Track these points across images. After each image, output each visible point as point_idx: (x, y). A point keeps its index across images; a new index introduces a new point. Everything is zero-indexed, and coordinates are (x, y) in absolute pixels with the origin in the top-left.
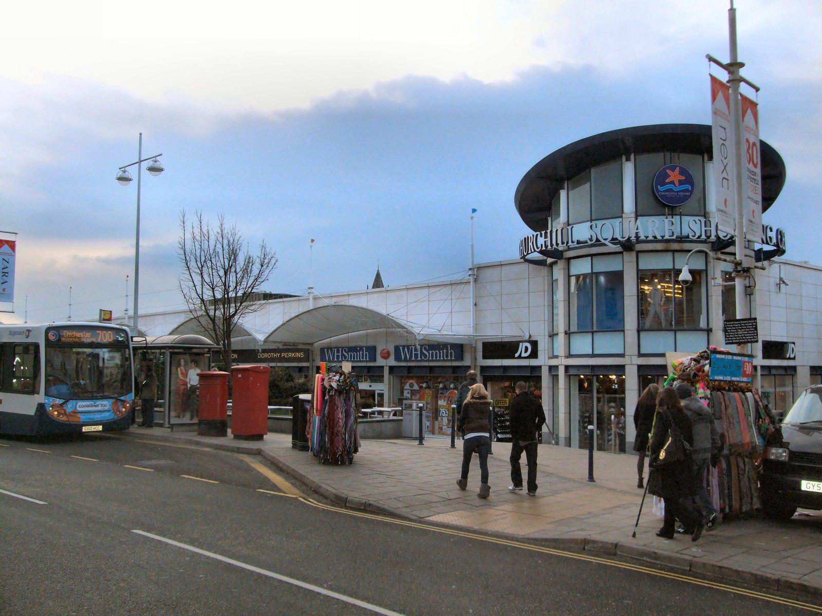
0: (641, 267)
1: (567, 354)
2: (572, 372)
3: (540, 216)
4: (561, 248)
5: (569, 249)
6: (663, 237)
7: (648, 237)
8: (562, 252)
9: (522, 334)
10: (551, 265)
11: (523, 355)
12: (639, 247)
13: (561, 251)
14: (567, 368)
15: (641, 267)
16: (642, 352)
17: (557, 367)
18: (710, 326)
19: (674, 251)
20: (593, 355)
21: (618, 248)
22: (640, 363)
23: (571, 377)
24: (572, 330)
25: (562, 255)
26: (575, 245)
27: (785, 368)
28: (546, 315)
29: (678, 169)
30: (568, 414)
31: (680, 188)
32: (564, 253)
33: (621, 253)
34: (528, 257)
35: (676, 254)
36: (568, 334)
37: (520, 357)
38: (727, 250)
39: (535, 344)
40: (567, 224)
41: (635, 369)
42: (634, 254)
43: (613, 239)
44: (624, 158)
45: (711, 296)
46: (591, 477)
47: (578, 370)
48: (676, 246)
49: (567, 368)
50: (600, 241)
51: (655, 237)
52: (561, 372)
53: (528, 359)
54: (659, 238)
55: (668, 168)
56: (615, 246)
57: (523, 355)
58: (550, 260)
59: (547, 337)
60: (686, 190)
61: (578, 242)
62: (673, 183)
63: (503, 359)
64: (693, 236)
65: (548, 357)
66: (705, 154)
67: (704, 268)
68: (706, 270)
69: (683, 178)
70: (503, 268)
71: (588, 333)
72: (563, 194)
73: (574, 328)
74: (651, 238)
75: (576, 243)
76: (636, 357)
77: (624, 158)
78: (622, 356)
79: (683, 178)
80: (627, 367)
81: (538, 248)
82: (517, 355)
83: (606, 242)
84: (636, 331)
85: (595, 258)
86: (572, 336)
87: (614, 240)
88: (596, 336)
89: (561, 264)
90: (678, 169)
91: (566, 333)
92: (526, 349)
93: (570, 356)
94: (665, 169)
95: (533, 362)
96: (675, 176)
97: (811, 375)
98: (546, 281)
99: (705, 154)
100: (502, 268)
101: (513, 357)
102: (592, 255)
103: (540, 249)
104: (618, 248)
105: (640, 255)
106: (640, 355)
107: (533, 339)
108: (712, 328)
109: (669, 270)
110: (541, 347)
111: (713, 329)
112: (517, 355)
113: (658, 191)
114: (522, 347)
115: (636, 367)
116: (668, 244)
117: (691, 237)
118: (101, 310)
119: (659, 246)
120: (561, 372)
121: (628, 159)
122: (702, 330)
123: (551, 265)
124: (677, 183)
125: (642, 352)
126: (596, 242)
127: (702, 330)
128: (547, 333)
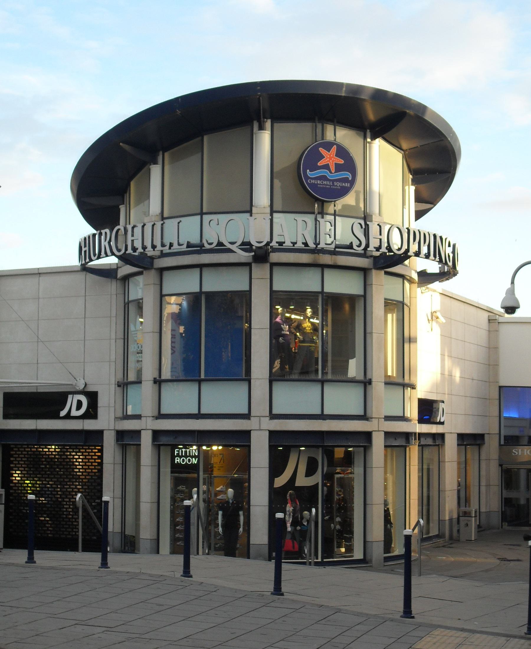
0: (275, 288)
1: (156, 414)
2: (164, 440)
3: (107, 201)
4: (150, 252)
5: (163, 255)
6: (294, 244)
7: (296, 243)
8: (152, 258)
9: (72, 382)
10: (126, 278)
11: (74, 413)
12: (274, 257)
13: (149, 257)
14: (156, 434)
15: (275, 288)
16: (275, 412)
17: (137, 434)
18: (369, 377)
19: (323, 267)
20: (199, 416)
21: (244, 256)
22: (272, 428)
23: (162, 448)
24: (163, 377)
25: (152, 264)
26: (184, 248)
27: (434, 436)
28: (113, 353)
29: (334, 148)
30: (156, 504)
31: (337, 176)
32: (155, 261)
33: (249, 265)
34: (96, 263)
35: (327, 272)
36: (158, 382)
37: (68, 416)
38: (396, 269)
39: (93, 397)
40: (160, 217)
41: (266, 436)
42: (153, 273)
43: (243, 244)
44: (256, 125)
45: (371, 333)
46: (408, 612)
47: (176, 438)
48: (326, 259)
49: (156, 434)
50: (223, 245)
51: (306, 244)
52: (146, 440)
53: (82, 420)
54: (312, 245)
55: (321, 145)
56: (247, 254)
57: (74, 413)
58: (128, 269)
59: (113, 387)
60: (345, 180)
61: (189, 245)
62: (327, 167)
63: (39, 419)
64: (357, 246)
65: (116, 418)
66: (368, 131)
67: (361, 293)
68: (364, 296)
69: (342, 162)
70: (42, 278)
71: (317, 383)
72: (155, 171)
73: (166, 374)
74: (300, 245)
75: (185, 246)
76: (383, 419)
77: (256, 125)
78: (247, 416)
79: (342, 162)
80: (253, 434)
81: (119, 250)
82: (63, 413)
83: (233, 247)
84: (268, 380)
85: (205, 271)
86: (164, 387)
87: (246, 246)
88: (205, 387)
89: (151, 276)
90: (334, 148)
91: (155, 381)
92: (79, 405)
93: (161, 416)
94: (316, 147)
95: (90, 425)
96: (330, 158)
97: (458, 445)
98: (114, 302)
99: (368, 131)
100: (40, 278)
101: (56, 416)
102: (201, 266)
103: (123, 251)
104: (244, 256)
105: (276, 269)
106: (273, 416)
107: (91, 389)
108: (370, 380)
109: (315, 294)
110: (102, 401)
111: (373, 380)
112: (63, 413)
113: (307, 177)
114: (72, 401)
115: (267, 433)
116: (316, 255)
117: (355, 247)
118: (385, 299)
119: (305, 258)
120: (146, 440)
121: (261, 128)
122: (353, 381)
123: (126, 278)
124: (333, 169)
125: (275, 412)
126: (216, 246)
127: (353, 381)
128: (113, 381)
